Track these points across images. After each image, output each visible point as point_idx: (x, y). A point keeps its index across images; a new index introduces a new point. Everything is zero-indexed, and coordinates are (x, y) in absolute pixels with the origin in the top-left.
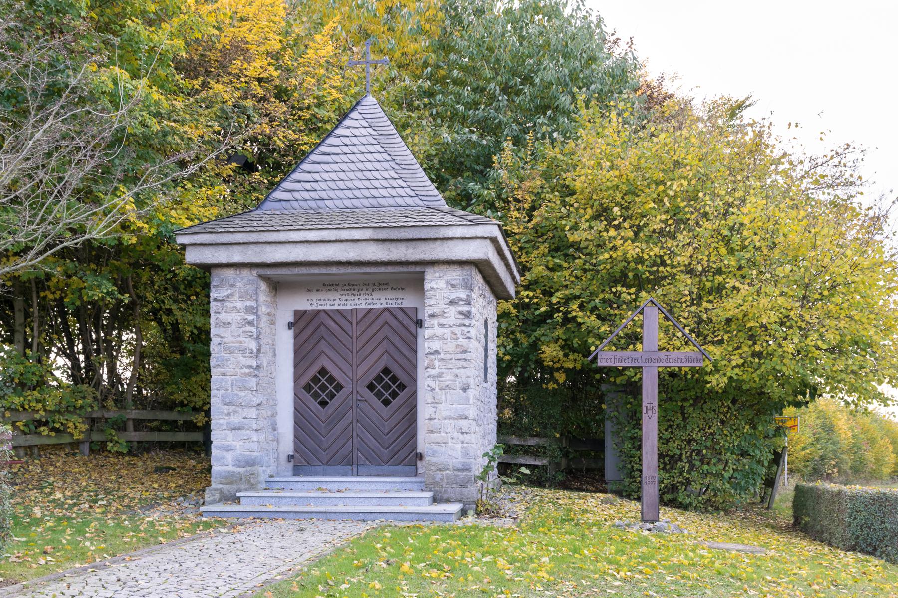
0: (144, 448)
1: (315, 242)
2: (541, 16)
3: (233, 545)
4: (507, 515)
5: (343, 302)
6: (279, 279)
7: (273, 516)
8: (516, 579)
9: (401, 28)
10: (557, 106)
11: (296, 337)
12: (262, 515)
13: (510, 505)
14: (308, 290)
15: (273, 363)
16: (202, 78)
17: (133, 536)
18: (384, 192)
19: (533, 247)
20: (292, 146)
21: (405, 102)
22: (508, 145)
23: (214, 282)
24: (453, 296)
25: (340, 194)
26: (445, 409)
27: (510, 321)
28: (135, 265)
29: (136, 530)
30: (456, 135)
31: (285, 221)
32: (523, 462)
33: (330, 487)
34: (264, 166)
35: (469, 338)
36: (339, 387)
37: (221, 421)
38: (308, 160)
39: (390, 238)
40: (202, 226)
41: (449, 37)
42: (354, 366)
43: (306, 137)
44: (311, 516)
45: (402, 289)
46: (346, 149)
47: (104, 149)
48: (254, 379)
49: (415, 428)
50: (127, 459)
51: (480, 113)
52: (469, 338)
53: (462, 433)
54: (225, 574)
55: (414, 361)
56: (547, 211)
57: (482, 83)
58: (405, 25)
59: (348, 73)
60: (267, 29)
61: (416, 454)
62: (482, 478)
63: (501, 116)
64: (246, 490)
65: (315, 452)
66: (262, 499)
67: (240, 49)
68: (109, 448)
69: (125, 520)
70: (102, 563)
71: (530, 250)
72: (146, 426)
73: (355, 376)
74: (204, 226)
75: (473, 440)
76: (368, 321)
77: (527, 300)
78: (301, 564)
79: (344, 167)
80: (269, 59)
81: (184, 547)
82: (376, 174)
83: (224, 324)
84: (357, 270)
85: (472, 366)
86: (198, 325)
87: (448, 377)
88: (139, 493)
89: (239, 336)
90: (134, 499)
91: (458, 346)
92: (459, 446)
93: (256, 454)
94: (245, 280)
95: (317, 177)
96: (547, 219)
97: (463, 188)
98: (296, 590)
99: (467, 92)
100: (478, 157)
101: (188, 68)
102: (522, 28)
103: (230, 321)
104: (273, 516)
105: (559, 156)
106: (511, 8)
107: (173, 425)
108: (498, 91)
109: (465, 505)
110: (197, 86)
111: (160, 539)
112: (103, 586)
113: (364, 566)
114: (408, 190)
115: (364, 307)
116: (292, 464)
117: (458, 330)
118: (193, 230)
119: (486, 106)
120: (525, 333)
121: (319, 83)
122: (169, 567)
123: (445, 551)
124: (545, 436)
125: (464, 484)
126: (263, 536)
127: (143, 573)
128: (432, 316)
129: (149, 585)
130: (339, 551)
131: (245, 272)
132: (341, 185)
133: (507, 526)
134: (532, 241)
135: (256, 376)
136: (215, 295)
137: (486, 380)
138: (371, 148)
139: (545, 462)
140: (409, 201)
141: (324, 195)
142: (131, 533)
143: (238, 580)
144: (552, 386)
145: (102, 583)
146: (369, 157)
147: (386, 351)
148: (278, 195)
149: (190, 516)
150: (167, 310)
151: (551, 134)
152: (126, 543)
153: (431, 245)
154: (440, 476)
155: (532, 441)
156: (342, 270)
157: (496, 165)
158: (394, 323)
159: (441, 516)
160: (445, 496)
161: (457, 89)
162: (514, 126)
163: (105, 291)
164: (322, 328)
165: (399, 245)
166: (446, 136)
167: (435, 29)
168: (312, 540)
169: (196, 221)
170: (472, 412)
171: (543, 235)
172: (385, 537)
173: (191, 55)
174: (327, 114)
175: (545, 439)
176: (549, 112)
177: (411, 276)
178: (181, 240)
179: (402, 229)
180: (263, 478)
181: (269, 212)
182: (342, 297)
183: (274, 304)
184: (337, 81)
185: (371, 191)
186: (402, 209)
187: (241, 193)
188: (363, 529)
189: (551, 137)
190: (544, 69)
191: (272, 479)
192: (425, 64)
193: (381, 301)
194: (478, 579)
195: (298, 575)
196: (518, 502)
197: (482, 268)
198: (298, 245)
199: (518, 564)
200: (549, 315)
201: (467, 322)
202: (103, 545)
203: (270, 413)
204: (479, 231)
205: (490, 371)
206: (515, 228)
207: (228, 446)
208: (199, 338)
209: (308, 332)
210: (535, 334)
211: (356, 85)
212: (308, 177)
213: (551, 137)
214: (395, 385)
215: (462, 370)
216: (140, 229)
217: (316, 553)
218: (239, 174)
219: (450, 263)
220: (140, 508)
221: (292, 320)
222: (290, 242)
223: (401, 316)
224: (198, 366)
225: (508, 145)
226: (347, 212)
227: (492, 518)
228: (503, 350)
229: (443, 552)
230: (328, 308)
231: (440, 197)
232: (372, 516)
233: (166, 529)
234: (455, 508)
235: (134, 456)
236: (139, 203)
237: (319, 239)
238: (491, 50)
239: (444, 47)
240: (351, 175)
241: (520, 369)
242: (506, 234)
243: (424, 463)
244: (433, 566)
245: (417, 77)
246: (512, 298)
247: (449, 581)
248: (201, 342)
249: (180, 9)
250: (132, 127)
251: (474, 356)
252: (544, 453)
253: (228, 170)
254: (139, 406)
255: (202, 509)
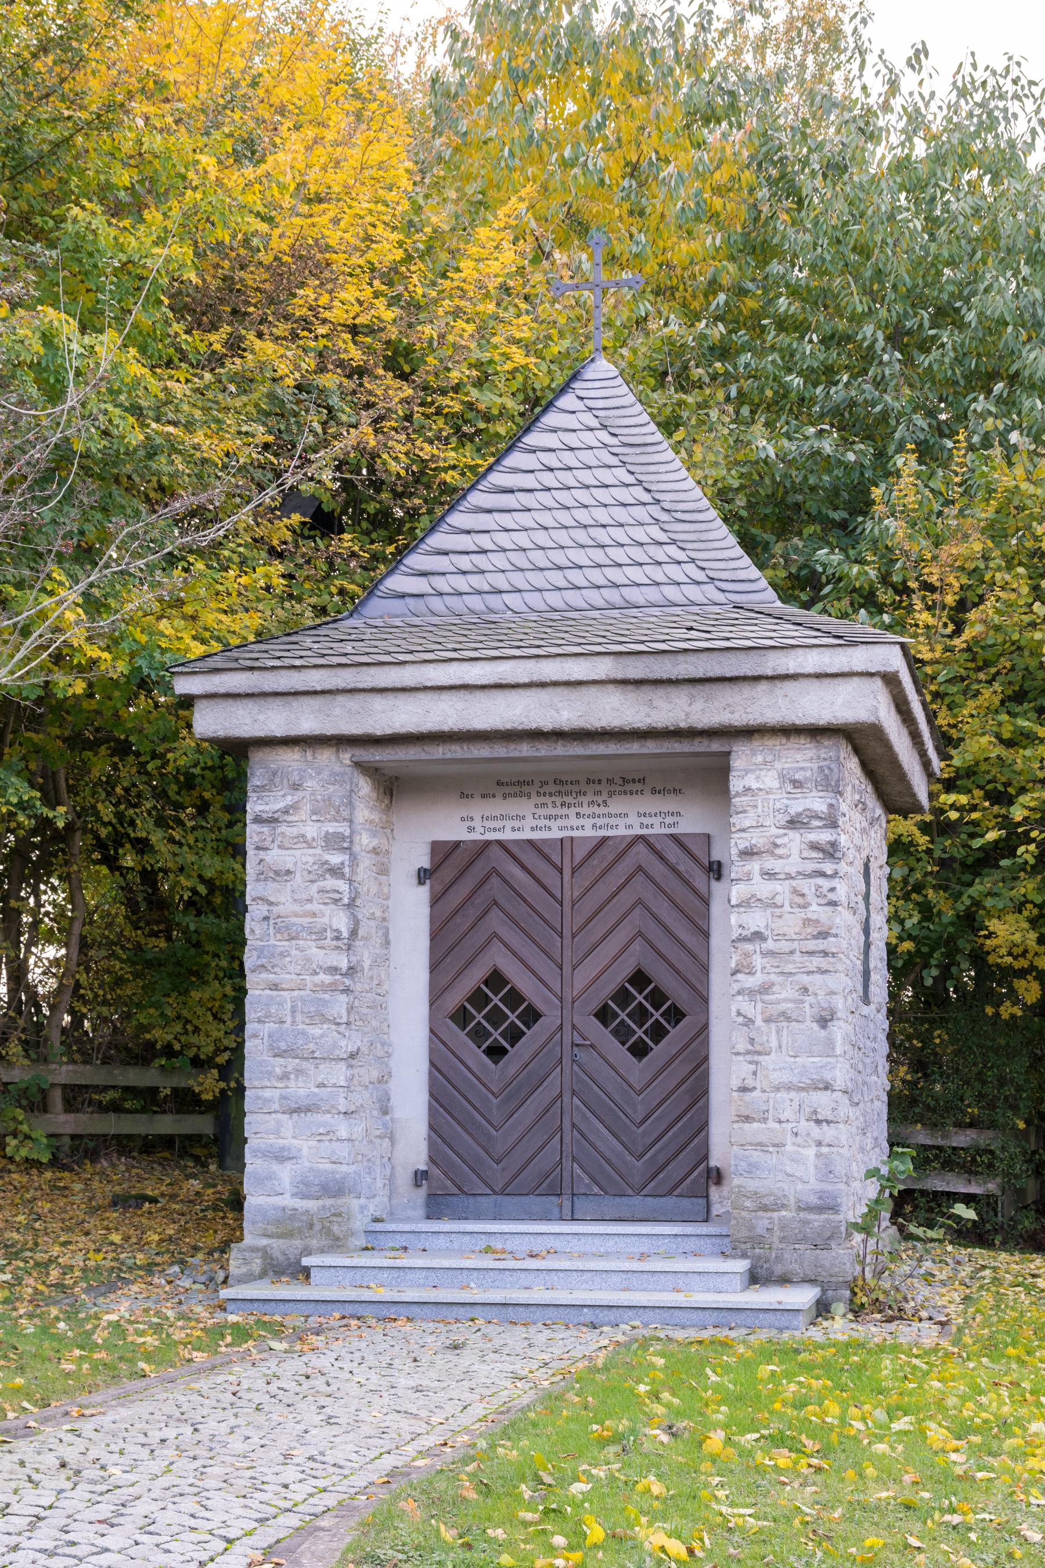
0: (86, 1151)
1: (483, 687)
2: (974, 173)
3: (306, 1385)
4: (924, 1314)
5: (542, 823)
6: (399, 772)
7: (385, 1312)
8: (980, 1475)
9: (659, 208)
10: (1017, 374)
11: (435, 901)
12: (360, 1310)
13: (926, 1291)
14: (463, 795)
15: (383, 960)
16: (229, 329)
17: (81, 1357)
18: (636, 574)
19: (965, 693)
20: (421, 475)
21: (664, 374)
22: (906, 463)
23: (256, 779)
24: (797, 807)
25: (537, 579)
26: (777, 1067)
27: (912, 861)
28: (75, 741)
29: (85, 1342)
30: (785, 443)
31: (415, 641)
32: (962, 1187)
33: (511, 1244)
34: (365, 521)
35: (833, 904)
36: (532, 1016)
37: (267, 1094)
38: (465, 505)
39: (652, 676)
40: (229, 654)
41: (766, 224)
42: (567, 968)
43: (453, 454)
44: (471, 1312)
45: (676, 791)
46: (548, 479)
47: (30, 489)
48: (343, 998)
49: (706, 1107)
50: (48, 1175)
51: (838, 394)
52: (833, 904)
53: (818, 1122)
54: (300, 1454)
55: (702, 956)
56: (998, 611)
57: (842, 325)
58: (671, 200)
59: (544, 309)
60: (369, 219)
61: (709, 1170)
62: (865, 1230)
63: (887, 398)
64: (322, 1251)
65: (473, 1165)
66: (359, 1273)
67: (310, 263)
68: (9, 1150)
69: (57, 1319)
70: (20, 1423)
71: (959, 699)
72: (91, 1102)
73: (567, 990)
74: (234, 654)
75: (843, 1139)
76: (598, 864)
77: (954, 815)
78: (466, 1430)
79: (546, 519)
80: (376, 283)
81: (195, 1386)
82: (618, 534)
83: (277, 873)
84: (576, 749)
85: (840, 967)
86: (209, 874)
87: (784, 993)
88: (80, 1256)
89: (310, 900)
90: (71, 1268)
91: (807, 922)
92: (811, 1152)
93: (344, 1168)
94: (325, 775)
95: (484, 541)
96: (997, 628)
97: (801, 560)
98: (472, 1495)
99: (809, 347)
100: (836, 492)
101: (196, 309)
102: (933, 199)
103: (290, 866)
104: (385, 1312)
105: (1024, 486)
106: (908, 157)
107: (149, 1099)
108: (881, 343)
109: (824, 1291)
110: (217, 347)
111: (142, 1365)
112: (30, 1481)
113: (617, 1438)
114: (690, 569)
115: (589, 832)
116: (423, 1192)
117: (807, 886)
118: (211, 663)
119: (853, 377)
120: (945, 889)
121: (483, 334)
122: (170, 1433)
123: (800, 1404)
124: (992, 1125)
125: (822, 1243)
126: (371, 1360)
127: (114, 1448)
128: (748, 853)
129: (132, 1477)
130: (552, 1400)
131: (325, 756)
132: (539, 558)
133: (927, 1342)
134: (963, 679)
135: (347, 991)
136: (259, 808)
137: (866, 999)
138: (605, 476)
139: (992, 1187)
140: (694, 593)
141: (500, 581)
142: (77, 1352)
143: (332, 1470)
144: (1007, 1010)
145: (28, 1471)
146: (602, 495)
147: (640, 934)
148: (397, 582)
149: (199, 1309)
150: (139, 840)
151: (1004, 436)
152: (68, 1375)
153: (747, 691)
154: (765, 1223)
155: (962, 1139)
156: (543, 750)
157: (879, 509)
158: (657, 869)
159: (770, 1317)
160: (778, 1270)
161: (784, 340)
162: (919, 420)
163: (14, 800)
164: (495, 880)
165: (673, 691)
166: (764, 446)
167: (733, 208)
168: (482, 1371)
169: (216, 647)
170: (840, 1074)
171: (987, 664)
172: (652, 1366)
173: (204, 280)
174: (499, 401)
175: (990, 1133)
176: (999, 387)
177: (701, 763)
178: (184, 686)
179: (681, 658)
180: (360, 1222)
181: (378, 622)
182: (541, 811)
183: (387, 828)
184: (524, 328)
185: (607, 571)
186: (677, 610)
187: (307, 578)
188: (591, 1345)
189: (1004, 443)
190: (986, 291)
191: (379, 1226)
192: (713, 286)
193: (628, 818)
194: (888, 1476)
195: (466, 1460)
196: (943, 1283)
197: (861, 742)
198: (446, 696)
199: (976, 1439)
200: (1006, 847)
201: (828, 868)
202: (19, 1381)
203: (375, 1074)
204: (858, 658)
205: (875, 977)
206: (924, 649)
207: (283, 1149)
208: (209, 903)
209: (462, 890)
210: (971, 891)
211: (561, 335)
212: (465, 542)
213: (1004, 443)
214: (658, 1013)
215: (818, 977)
216: (94, 662)
217: (496, 1402)
218: (304, 537)
219: (788, 731)
220: (87, 1291)
221: (425, 863)
222: (426, 689)
223: (673, 854)
224: (207, 965)
225: (906, 463)
226: (554, 620)
227: (890, 1320)
228: (897, 928)
229: (794, 1406)
230: (507, 835)
231: (764, 583)
232: (612, 1315)
233: (151, 1341)
234: (803, 1297)
235: (64, 1168)
236: (93, 605)
237: (491, 681)
238: (864, 251)
239: (757, 248)
240: (562, 537)
241: (935, 972)
242: (914, 663)
243: (725, 1189)
244: (778, 1441)
245: (692, 317)
246: (920, 810)
247: (818, 1478)
248: (213, 911)
249: (184, 178)
250: (85, 441)
251: (844, 944)
252: (990, 1166)
253: (281, 530)
254: (77, 1057)
255: (225, 1293)
